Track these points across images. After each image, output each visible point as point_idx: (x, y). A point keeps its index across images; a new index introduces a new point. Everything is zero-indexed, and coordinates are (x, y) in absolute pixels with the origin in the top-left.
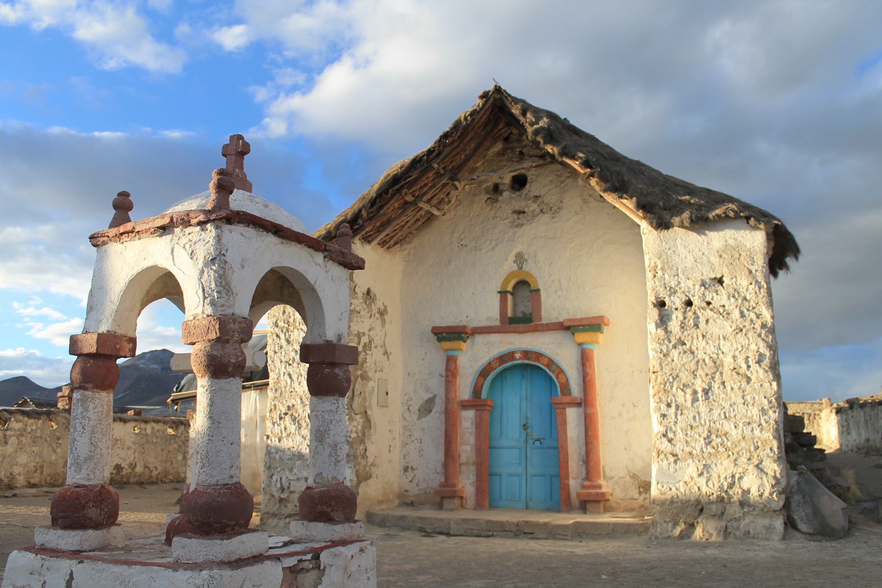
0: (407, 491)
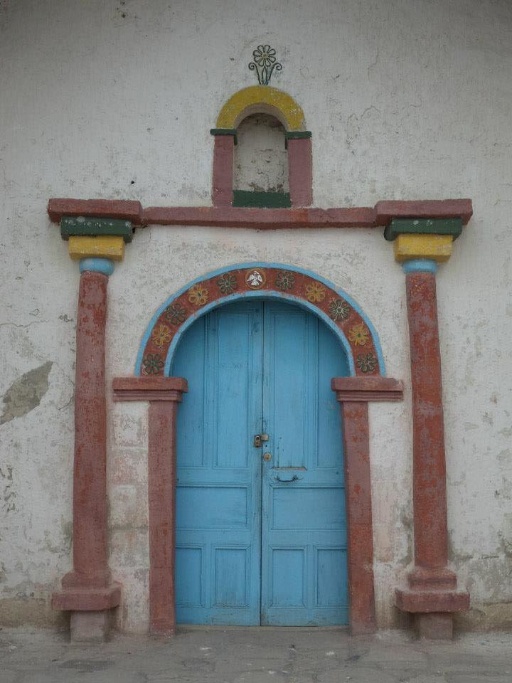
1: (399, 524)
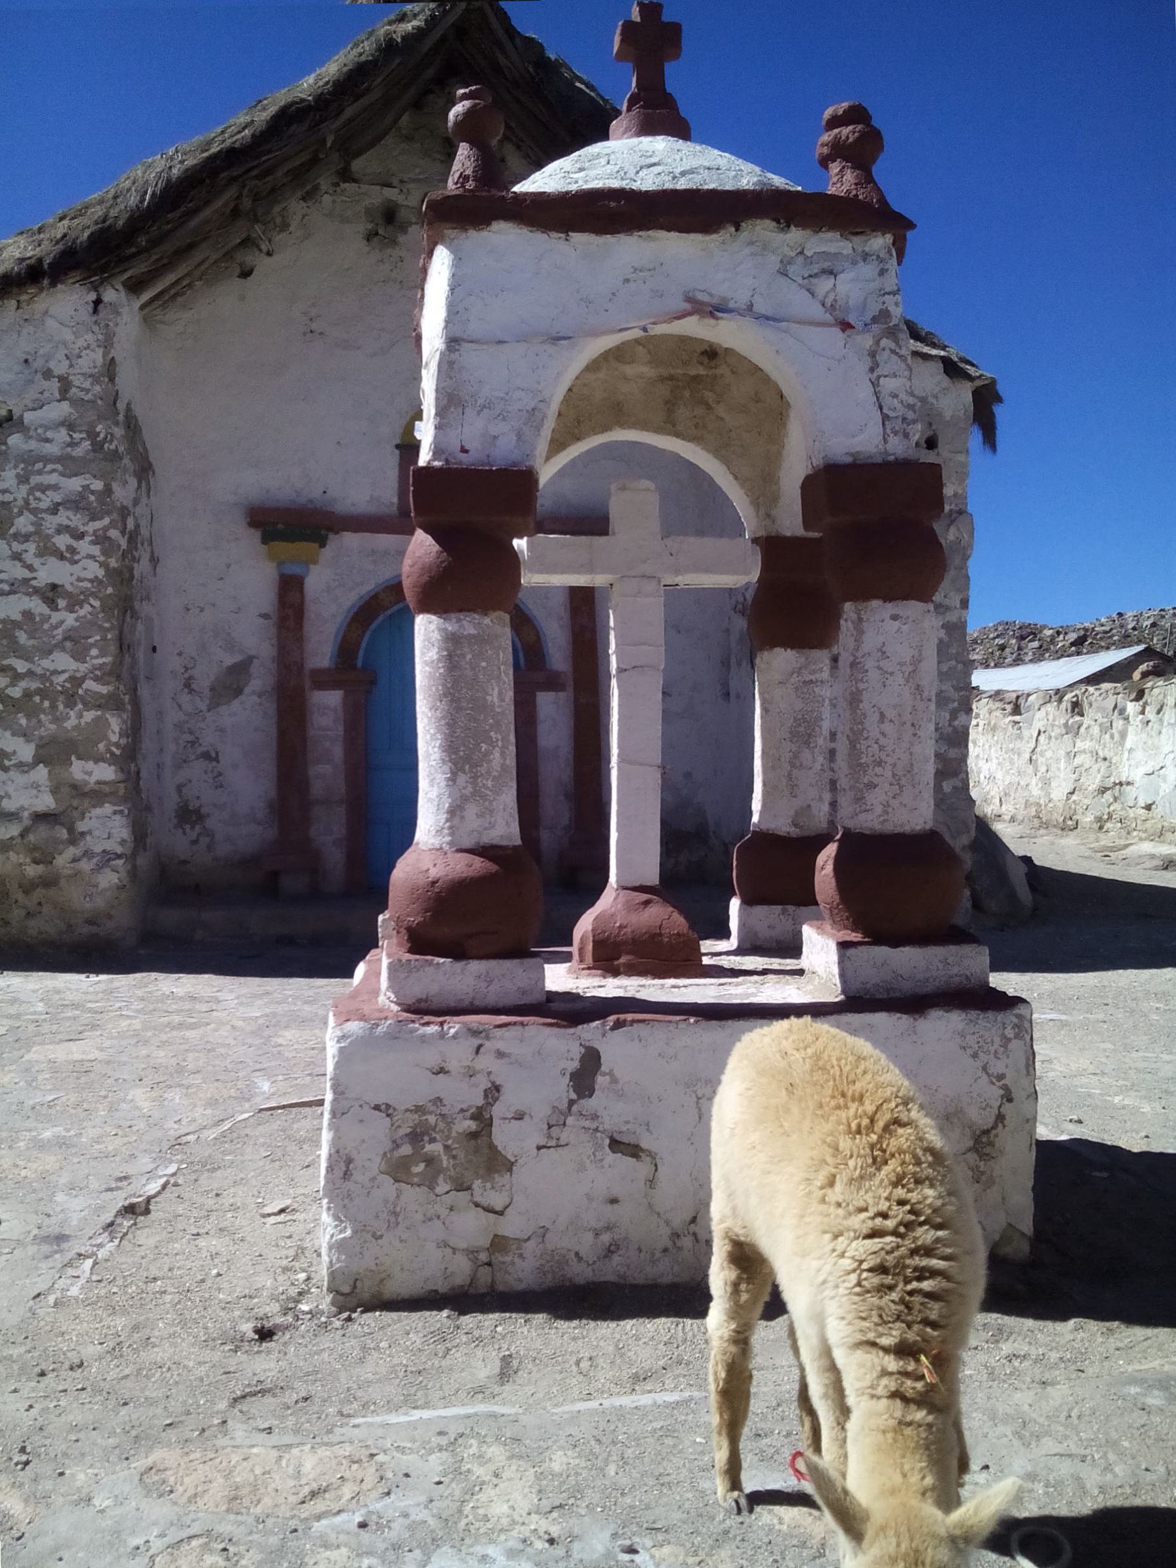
0: (184, 862)
1: (562, 798)
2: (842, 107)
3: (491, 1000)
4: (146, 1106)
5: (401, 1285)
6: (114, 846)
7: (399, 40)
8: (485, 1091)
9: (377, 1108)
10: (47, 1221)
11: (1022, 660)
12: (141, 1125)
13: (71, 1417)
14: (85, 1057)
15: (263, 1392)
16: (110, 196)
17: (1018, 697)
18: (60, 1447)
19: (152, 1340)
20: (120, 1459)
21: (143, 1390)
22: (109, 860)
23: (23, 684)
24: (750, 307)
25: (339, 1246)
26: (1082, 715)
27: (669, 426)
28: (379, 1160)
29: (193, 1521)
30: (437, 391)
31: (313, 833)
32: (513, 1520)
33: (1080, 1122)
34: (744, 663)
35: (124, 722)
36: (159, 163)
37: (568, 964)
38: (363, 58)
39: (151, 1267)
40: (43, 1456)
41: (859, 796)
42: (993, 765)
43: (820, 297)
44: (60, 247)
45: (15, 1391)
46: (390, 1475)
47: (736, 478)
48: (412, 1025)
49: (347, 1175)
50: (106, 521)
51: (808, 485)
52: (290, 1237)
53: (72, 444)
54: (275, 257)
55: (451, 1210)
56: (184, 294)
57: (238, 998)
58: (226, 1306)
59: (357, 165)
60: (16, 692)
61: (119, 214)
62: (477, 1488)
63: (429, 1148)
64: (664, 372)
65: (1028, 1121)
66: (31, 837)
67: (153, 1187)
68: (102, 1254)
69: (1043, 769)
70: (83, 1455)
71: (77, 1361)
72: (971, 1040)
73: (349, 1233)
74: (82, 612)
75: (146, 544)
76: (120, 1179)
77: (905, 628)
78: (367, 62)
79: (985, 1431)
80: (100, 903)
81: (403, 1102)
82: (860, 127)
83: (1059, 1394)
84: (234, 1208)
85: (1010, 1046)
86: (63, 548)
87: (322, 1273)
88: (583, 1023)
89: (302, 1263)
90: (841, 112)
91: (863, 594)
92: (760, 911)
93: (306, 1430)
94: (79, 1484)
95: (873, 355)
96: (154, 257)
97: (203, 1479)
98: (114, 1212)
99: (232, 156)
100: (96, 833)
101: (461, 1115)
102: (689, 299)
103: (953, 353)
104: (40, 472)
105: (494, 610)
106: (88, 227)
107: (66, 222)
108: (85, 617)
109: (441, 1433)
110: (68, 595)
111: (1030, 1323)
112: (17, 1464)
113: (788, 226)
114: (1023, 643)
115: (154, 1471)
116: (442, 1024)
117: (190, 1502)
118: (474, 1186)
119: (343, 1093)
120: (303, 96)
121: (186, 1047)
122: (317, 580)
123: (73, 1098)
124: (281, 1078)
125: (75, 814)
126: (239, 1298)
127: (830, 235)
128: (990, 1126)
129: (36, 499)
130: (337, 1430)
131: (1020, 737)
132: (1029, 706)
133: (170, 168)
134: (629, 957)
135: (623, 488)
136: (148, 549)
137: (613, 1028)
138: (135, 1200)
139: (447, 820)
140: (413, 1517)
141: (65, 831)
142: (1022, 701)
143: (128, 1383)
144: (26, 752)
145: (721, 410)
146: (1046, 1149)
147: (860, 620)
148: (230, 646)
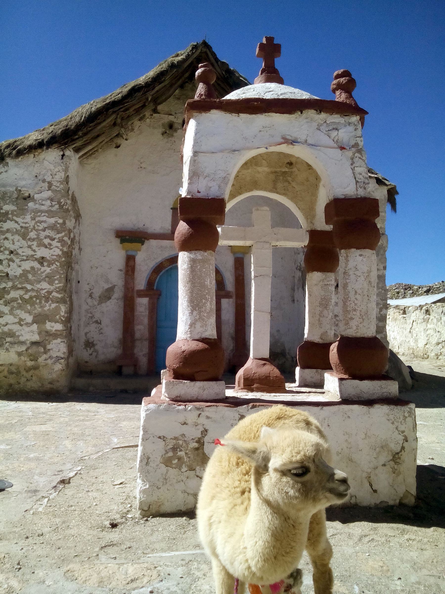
0: (87, 362)
1: (230, 339)
2: (340, 71)
3: (205, 397)
4: (69, 447)
5: (167, 508)
6: (61, 355)
7: (176, 63)
8: (202, 432)
9: (160, 437)
10: (31, 485)
11: (406, 298)
12: (67, 453)
13: (37, 553)
14: (47, 430)
15: (113, 545)
16: (69, 118)
17: (405, 308)
18: (33, 563)
19: (70, 526)
20: (56, 567)
21: (66, 544)
22: (58, 360)
23: (30, 294)
24: (306, 141)
25: (143, 492)
26: (430, 315)
27: (274, 190)
28: (160, 458)
29: (85, 590)
30: (189, 170)
31: (136, 351)
32: (211, 591)
33: (433, 459)
34: (300, 288)
35: (67, 308)
36: (88, 106)
37: (233, 390)
38: (163, 69)
39: (70, 502)
40: (26, 566)
41: (347, 322)
42: (395, 333)
43: (332, 138)
44: (51, 135)
45: (16, 543)
46: (162, 574)
47: (299, 209)
48: (174, 406)
49: (147, 464)
50: (63, 234)
51: (328, 207)
52: (124, 492)
53: (52, 206)
54: (128, 141)
55: (187, 478)
56: (95, 154)
57: (105, 411)
58: (99, 515)
59: (160, 108)
60: (27, 297)
61: (72, 124)
62: (197, 580)
63: (179, 453)
64: (273, 170)
65: (414, 449)
66: (30, 351)
67: (72, 474)
68: (51, 497)
69: (415, 335)
70: (42, 566)
71: (41, 533)
72: (391, 417)
73: (148, 486)
74: (53, 267)
75: (77, 243)
76: (59, 471)
77: (364, 259)
78: (164, 71)
79: (399, 565)
80: (54, 376)
81: (169, 436)
82: (347, 78)
83: (428, 554)
84: (102, 482)
85: (407, 420)
86: (47, 244)
87: (137, 503)
88: (240, 406)
89: (129, 501)
90: (340, 73)
91: (348, 246)
92: (307, 371)
93: (130, 558)
94: (40, 576)
95: (352, 159)
96: (84, 140)
97: (89, 575)
98: (56, 483)
99: (114, 104)
100: (54, 349)
101: (192, 441)
102: (283, 138)
103: (380, 176)
104: (39, 216)
105: (209, 250)
106: (61, 128)
107: (53, 127)
108: (53, 269)
109: (182, 560)
110: (48, 261)
111: (415, 528)
112: (16, 569)
113: (321, 112)
114: (406, 291)
115: (69, 571)
116: (185, 405)
117: (83, 583)
118: (197, 469)
119: (147, 432)
120: (140, 83)
121: (85, 427)
122: (140, 257)
123: (42, 444)
124: (121, 437)
125: (47, 342)
126: (104, 513)
127: (336, 116)
128: (399, 451)
129: (38, 226)
130: (142, 559)
131: (406, 323)
132: (409, 311)
133: (91, 108)
134: (258, 385)
135: (258, 210)
136: (78, 245)
137: (251, 408)
138: (65, 478)
139: (189, 328)
140: (171, 589)
141: (42, 349)
142: (406, 309)
143: (61, 541)
144: (29, 319)
145: (294, 184)
146: (421, 469)
147: (347, 256)
148: (107, 281)
